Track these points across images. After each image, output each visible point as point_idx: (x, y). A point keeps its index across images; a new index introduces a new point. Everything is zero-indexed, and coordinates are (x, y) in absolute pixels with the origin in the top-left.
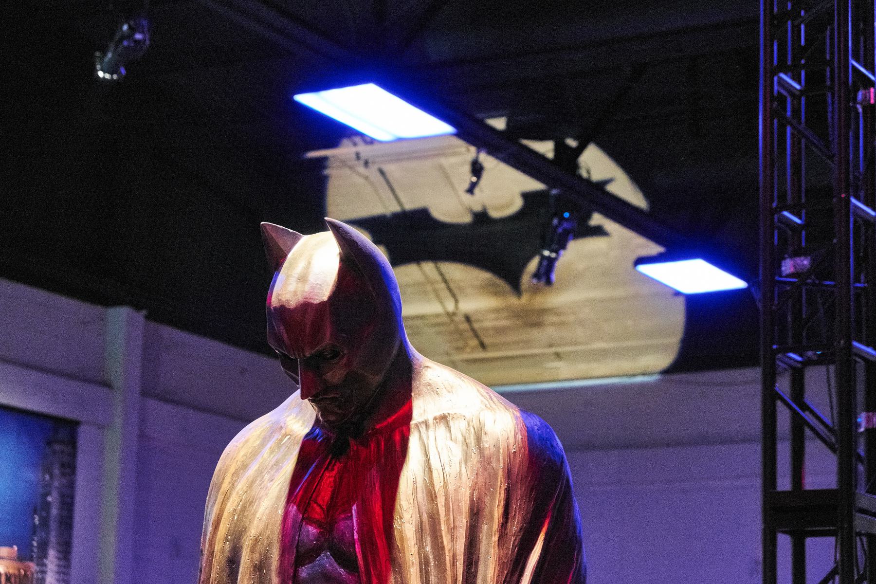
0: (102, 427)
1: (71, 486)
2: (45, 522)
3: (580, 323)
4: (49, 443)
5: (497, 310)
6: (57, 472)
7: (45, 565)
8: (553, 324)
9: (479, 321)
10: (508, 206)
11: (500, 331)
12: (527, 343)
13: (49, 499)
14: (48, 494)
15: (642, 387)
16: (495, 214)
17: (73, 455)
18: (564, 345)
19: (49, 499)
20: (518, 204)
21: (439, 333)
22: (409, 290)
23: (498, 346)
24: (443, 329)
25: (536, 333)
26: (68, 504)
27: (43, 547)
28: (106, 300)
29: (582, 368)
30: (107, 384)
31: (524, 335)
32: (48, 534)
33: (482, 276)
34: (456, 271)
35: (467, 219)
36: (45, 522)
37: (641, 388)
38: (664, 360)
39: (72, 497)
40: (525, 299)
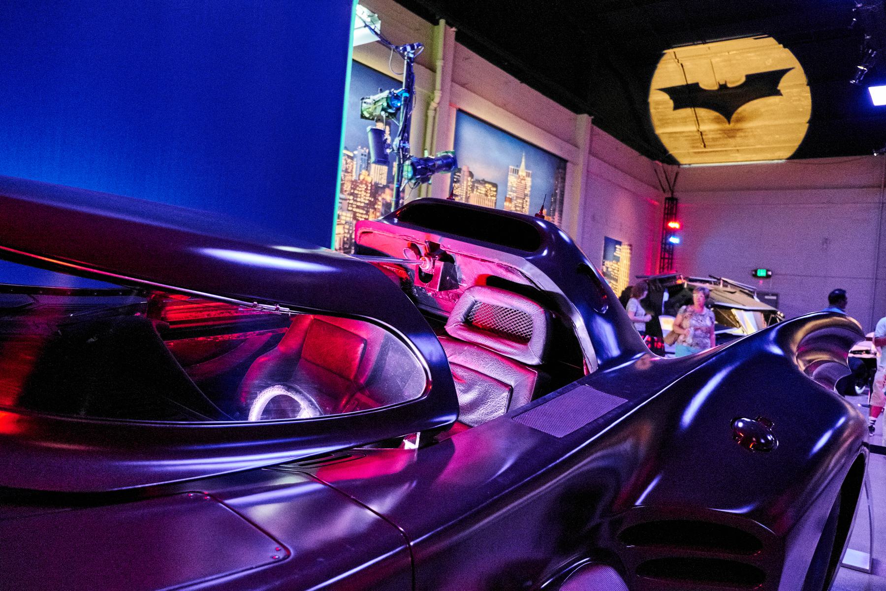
0: (575, 164)
1: (564, 187)
2: (555, 202)
3: (754, 136)
4: (558, 168)
5: (718, 130)
6: (560, 181)
7: (554, 219)
8: (741, 137)
9: (706, 135)
10: (737, 81)
11: (714, 140)
12: (725, 145)
13: (557, 191)
14: (556, 189)
15: (777, 165)
16: (729, 85)
17: (565, 174)
18: (742, 146)
19: (557, 191)
20: (743, 80)
21: (686, 140)
22: (678, 121)
23: (711, 146)
24: (688, 138)
25: (731, 141)
26: (562, 195)
27: (554, 210)
28: (577, 110)
29: (749, 156)
30: (576, 146)
31: (725, 141)
32: (556, 206)
33: (714, 114)
34: (702, 112)
35: (716, 88)
36: (555, 202)
37: (777, 166)
38: (789, 154)
39: (564, 192)
40: (732, 124)
